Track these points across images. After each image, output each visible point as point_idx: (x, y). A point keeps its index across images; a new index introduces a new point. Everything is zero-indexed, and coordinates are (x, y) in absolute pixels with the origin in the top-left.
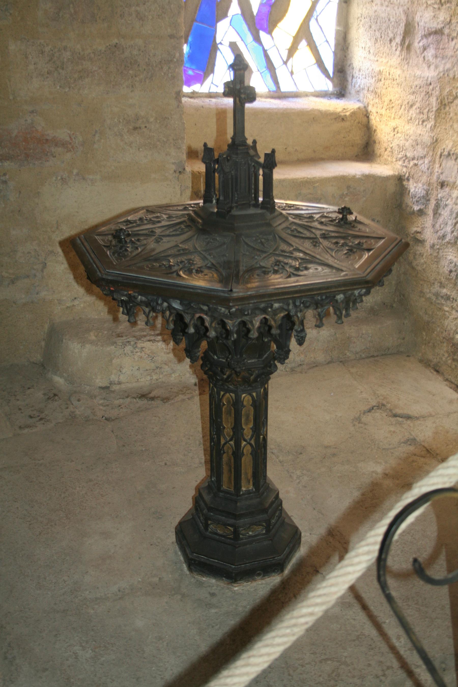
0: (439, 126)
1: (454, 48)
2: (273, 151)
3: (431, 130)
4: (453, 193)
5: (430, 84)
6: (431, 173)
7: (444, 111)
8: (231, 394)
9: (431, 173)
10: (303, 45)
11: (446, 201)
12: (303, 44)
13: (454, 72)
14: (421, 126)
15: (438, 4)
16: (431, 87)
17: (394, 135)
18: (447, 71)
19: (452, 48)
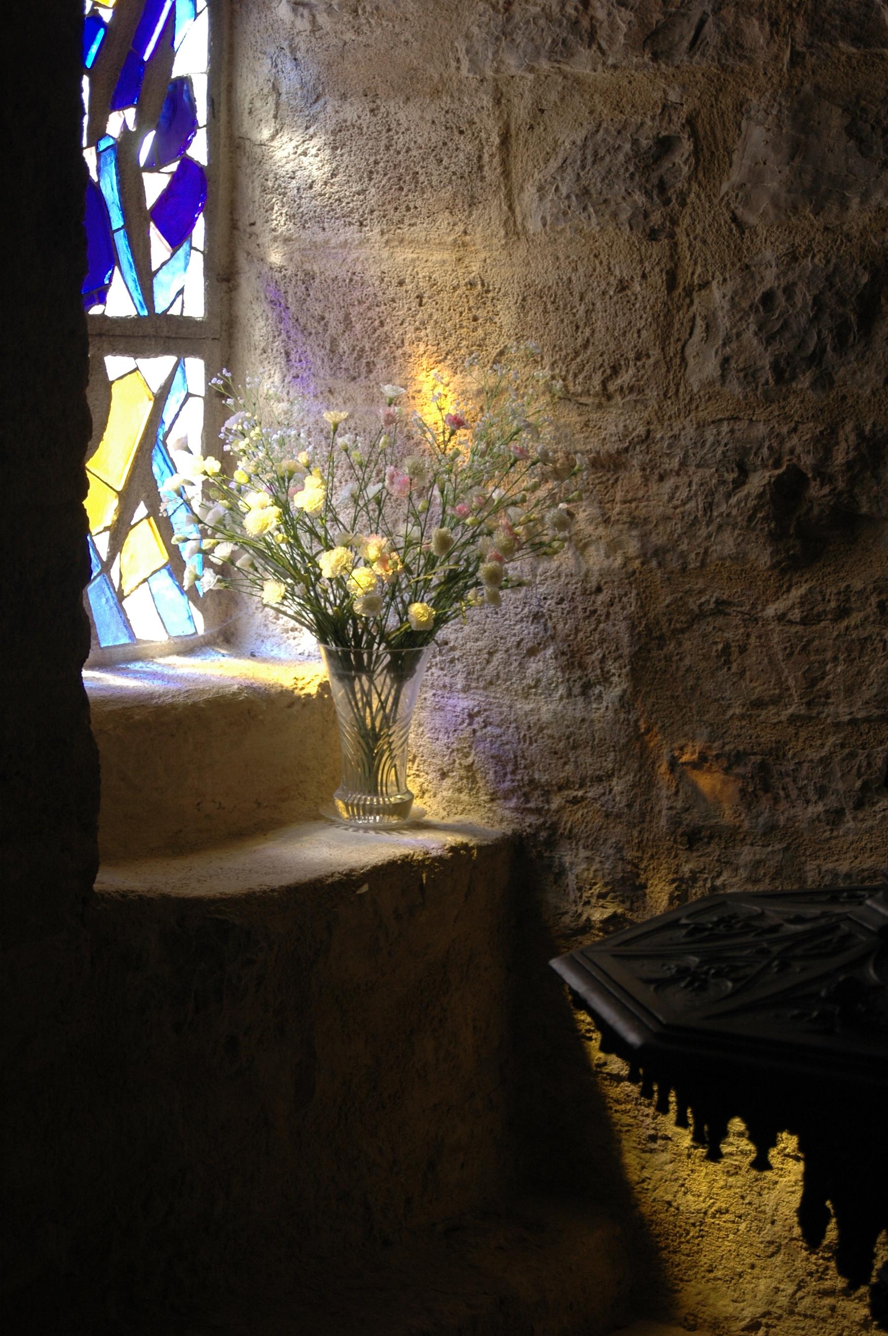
0: (648, 693)
1: (671, 499)
2: (205, 459)
3: (623, 706)
4: (738, 855)
5: (599, 590)
6: (643, 815)
7: (662, 653)
8: (96, 180)
9: (643, 815)
10: (198, 11)
11: (714, 879)
12: (198, 11)
13: (683, 555)
14: (580, 699)
15: (597, 395)
16: (600, 598)
17: (474, 731)
18: (656, 553)
19: (666, 497)
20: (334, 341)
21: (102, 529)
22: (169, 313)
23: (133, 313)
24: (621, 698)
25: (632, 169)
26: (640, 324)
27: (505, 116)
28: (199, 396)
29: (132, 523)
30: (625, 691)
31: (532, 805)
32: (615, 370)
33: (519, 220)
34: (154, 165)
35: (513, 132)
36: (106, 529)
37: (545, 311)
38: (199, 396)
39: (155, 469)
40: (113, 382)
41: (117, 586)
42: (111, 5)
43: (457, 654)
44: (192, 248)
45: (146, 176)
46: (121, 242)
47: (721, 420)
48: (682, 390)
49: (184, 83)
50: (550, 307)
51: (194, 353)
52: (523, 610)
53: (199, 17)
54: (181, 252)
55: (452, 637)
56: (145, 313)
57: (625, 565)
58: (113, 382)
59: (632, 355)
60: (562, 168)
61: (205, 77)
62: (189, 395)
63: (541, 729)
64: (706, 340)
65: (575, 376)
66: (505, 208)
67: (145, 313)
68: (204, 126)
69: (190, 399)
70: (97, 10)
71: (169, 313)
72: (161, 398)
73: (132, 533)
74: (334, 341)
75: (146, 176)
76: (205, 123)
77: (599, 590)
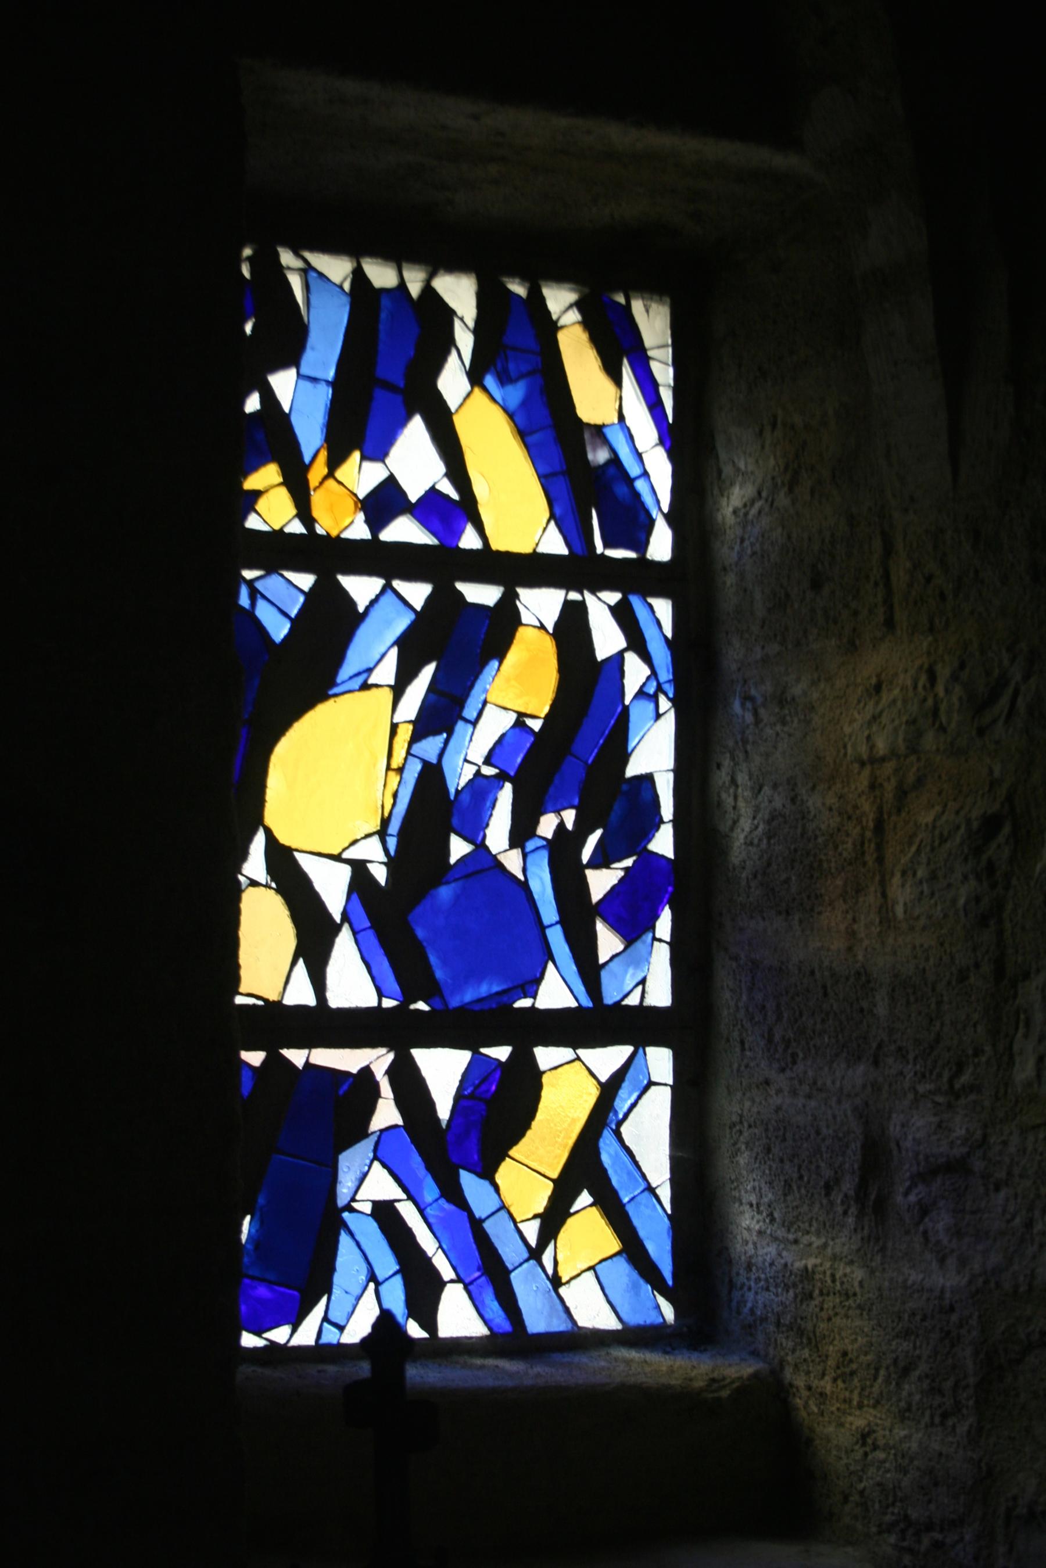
1: (1004, 1211)
20: (770, 1030)
21: (530, 1216)
22: (624, 1003)
23: (573, 1004)
24: (969, 1432)
25: (966, 851)
26: (976, 1016)
27: (878, 801)
28: (666, 1085)
29: (572, 1210)
30: (971, 1426)
31: (905, 1544)
32: (960, 1067)
33: (890, 906)
34: (602, 859)
35: (886, 817)
36: (535, 1217)
37: (908, 1003)
38: (666, 1085)
39: (605, 1158)
40: (544, 1072)
41: (550, 1271)
42: (543, 715)
43: (854, 1366)
44: (654, 939)
45: (590, 873)
46: (556, 937)
47: (1039, 1126)
48: (1010, 1091)
49: (648, 779)
50: (912, 999)
51: (658, 1042)
52: (898, 1324)
53: (663, 719)
54: (639, 946)
55: (850, 1348)
56: (587, 1002)
57: (970, 1282)
58: (544, 1072)
59: (970, 1052)
60: (918, 851)
61: (671, 776)
62: (651, 1084)
63: (912, 1460)
64: (1026, 1036)
65: (931, 1073)
66: (879, 895)
67: (587, 1002)
68: (670, 821)
69: (653, 1088)
70: (524, 722)
71: (624, 1003)
72: (609, 1089)
73: (570, 1221)
74: (770, 1030)
75: (590, 873)
76: (671, 817)
77: (952, 1309)
